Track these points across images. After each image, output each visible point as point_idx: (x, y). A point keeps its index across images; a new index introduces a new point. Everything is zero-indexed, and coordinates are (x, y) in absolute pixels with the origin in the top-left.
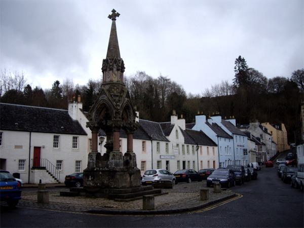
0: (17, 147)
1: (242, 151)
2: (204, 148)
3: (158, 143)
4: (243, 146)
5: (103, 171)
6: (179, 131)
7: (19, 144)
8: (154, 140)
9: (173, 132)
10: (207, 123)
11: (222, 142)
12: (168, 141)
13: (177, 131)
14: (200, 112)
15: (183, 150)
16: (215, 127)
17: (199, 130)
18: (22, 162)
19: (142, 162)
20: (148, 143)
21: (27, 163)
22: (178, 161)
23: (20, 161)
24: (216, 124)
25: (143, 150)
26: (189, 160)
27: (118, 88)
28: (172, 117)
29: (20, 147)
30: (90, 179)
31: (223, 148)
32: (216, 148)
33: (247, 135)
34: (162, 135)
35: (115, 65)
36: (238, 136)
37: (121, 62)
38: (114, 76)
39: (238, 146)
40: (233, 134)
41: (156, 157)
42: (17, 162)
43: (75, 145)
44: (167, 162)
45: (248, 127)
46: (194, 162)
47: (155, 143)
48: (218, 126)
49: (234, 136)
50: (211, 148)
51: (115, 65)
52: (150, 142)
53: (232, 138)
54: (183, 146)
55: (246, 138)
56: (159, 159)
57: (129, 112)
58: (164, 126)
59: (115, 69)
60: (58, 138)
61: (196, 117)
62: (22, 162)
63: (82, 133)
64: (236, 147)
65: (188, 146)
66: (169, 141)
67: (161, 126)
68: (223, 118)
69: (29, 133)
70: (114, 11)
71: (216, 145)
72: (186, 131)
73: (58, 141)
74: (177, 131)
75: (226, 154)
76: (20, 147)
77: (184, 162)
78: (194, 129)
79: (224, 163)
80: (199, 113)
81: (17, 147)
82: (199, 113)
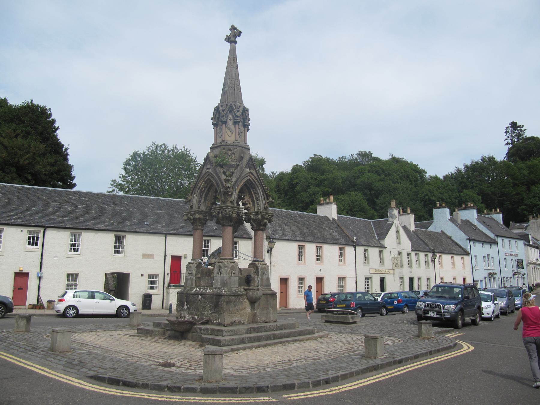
0: (145, 256)
1: (515, 262)
2: (446, 258)
3: (366, 250)
4: (516, 255)
5: (203, 295)
6: (401, 231)
7: (148, 261)
8: (359, 245)
9: (393, 231)
10: (453, 220)
11: (477, 249)
12: (384, 247)
13: (398, 232)
14: (440, 205)
15: (410, 261)
16: (466, 226)
17: (439, 231)
18: (153, 278)
19: (69, 275)
20: (349, 251)
21: (160, 280)
22: (401, 278)
23: (150, 276)
24: (468, 221)
25: (341, 260)
26: (419, 276)
27: (234, 153)
28: (435, 211)
29: (151, 256)
30: (185, 307)
31: (480, 259)
32: (467, 259)
33: (525, 238)
34: (374, 238)
35: (230, 116)
36: (506, 240)
37: (241, 109)
38: (230, 134)
39: (506, 254)
40: (497, 236)
41: (364, 271)
42: (146, 279)
43: (341, 258)
44: (382, 280)
45: (527, 227)
46: (428, 279)
47: (360, 250)
48: (471, 224)
49: (499, 240)
50: (458, 258)
51: (230, 116)
52: (353, 248)
53: (496, 243)
54: (409, 254)
55: (521, 243)
56: (368, 275)
57: (256, 193)
58: (378, 226)
59: (230, 123)
60: (208, 242)
61: (435, 211)
62: (153, 278)
63: (245, 236)
64: (502, 256)
65: (417, 255)
66: (385, 248)
67: (374, 225)
68: (480, 212)
69: (161, 239)
70: (233, 28)
71: (468, 254)
72: (415, 232)
73: (208, 247)
74: (398, 232)
75: (485, 268)
76: (151, 256)
77: (411, 280)
78: (431, 229)
79: (481, 281)
80: (438, 205)
81: (145, 256)
82: (438, 205)
